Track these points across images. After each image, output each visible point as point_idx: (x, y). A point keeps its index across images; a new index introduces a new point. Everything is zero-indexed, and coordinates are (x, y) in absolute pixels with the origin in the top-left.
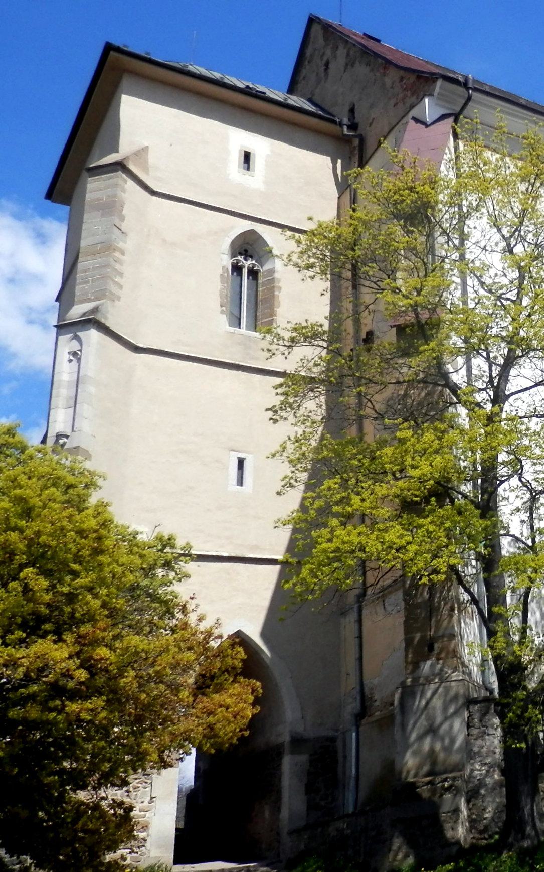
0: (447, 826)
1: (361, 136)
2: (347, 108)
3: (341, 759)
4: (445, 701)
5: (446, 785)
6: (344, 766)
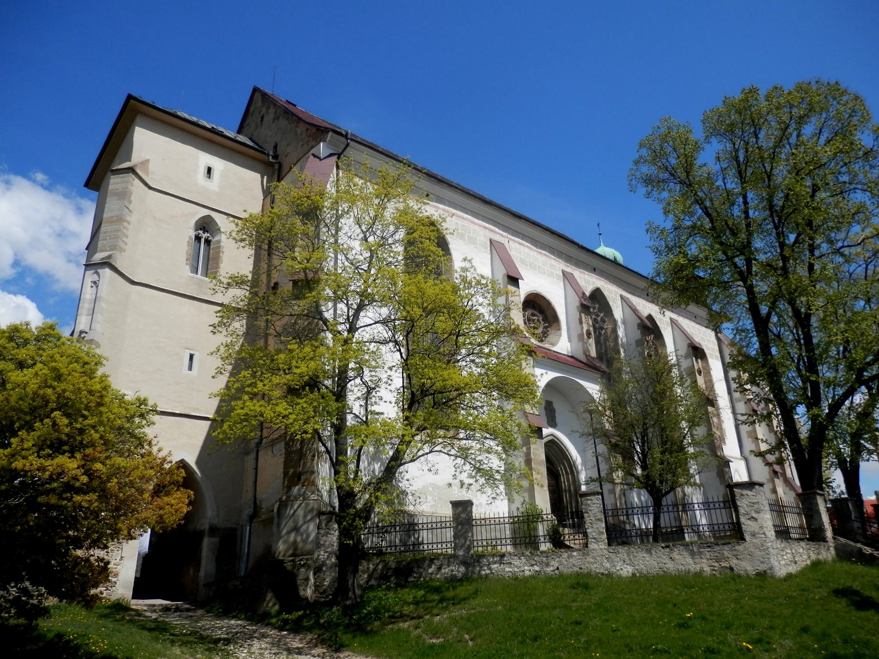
0: (301, 588)
3: (239, 542)
4: (305, 512)
5: (302, 563)
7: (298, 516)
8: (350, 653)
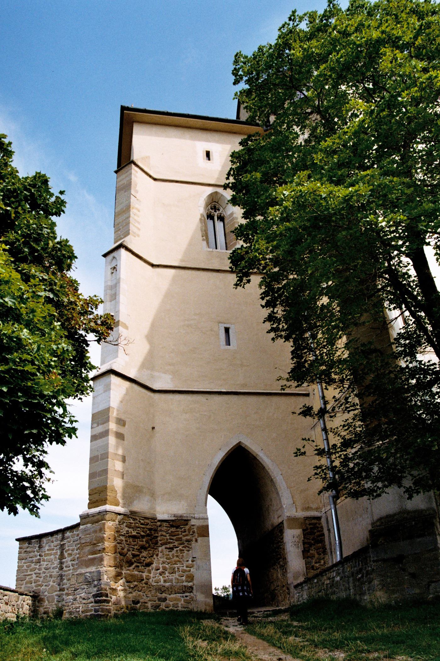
3: (326, 532)
6: (329, 536)
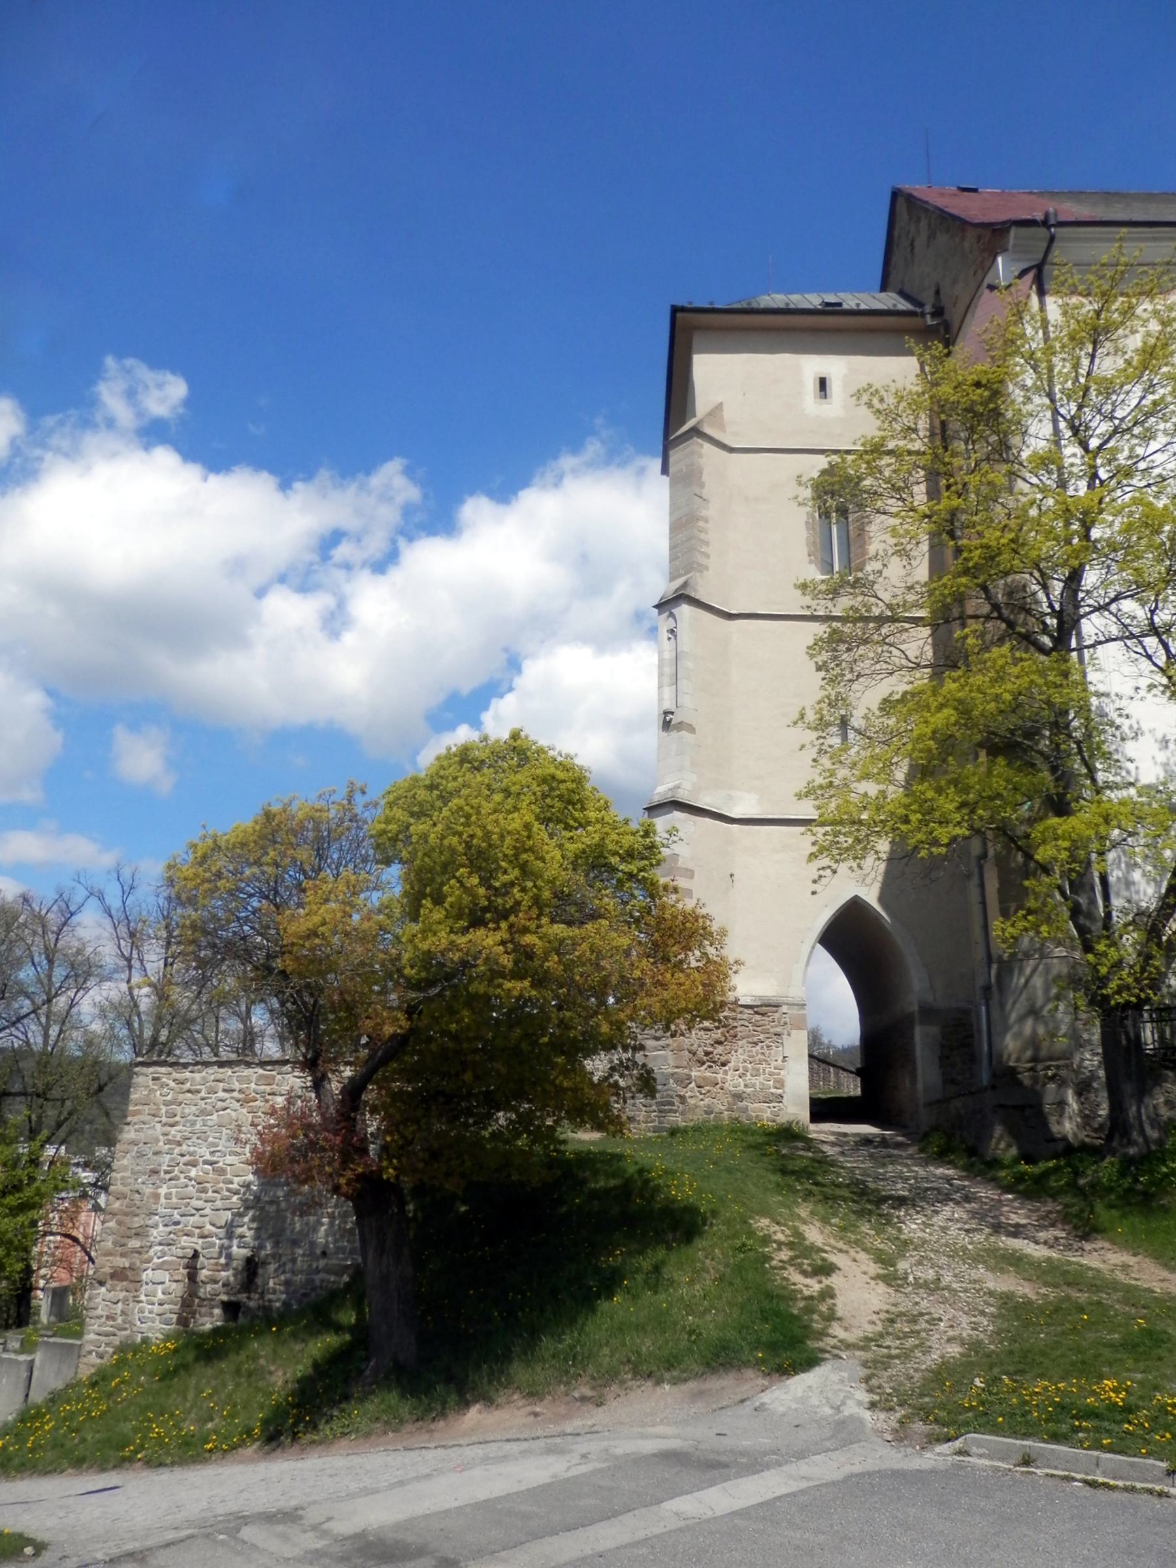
0: (1053, 1119)
1: (946, 321)
2: (932, 291)
4: (1046, 981)
5: (1050, 1073)
7: (1035, 988)
8: (1107, 1245)
